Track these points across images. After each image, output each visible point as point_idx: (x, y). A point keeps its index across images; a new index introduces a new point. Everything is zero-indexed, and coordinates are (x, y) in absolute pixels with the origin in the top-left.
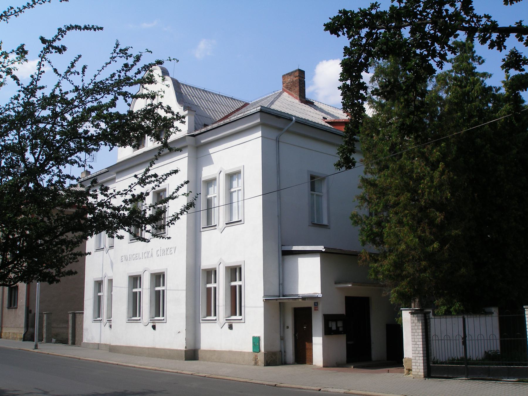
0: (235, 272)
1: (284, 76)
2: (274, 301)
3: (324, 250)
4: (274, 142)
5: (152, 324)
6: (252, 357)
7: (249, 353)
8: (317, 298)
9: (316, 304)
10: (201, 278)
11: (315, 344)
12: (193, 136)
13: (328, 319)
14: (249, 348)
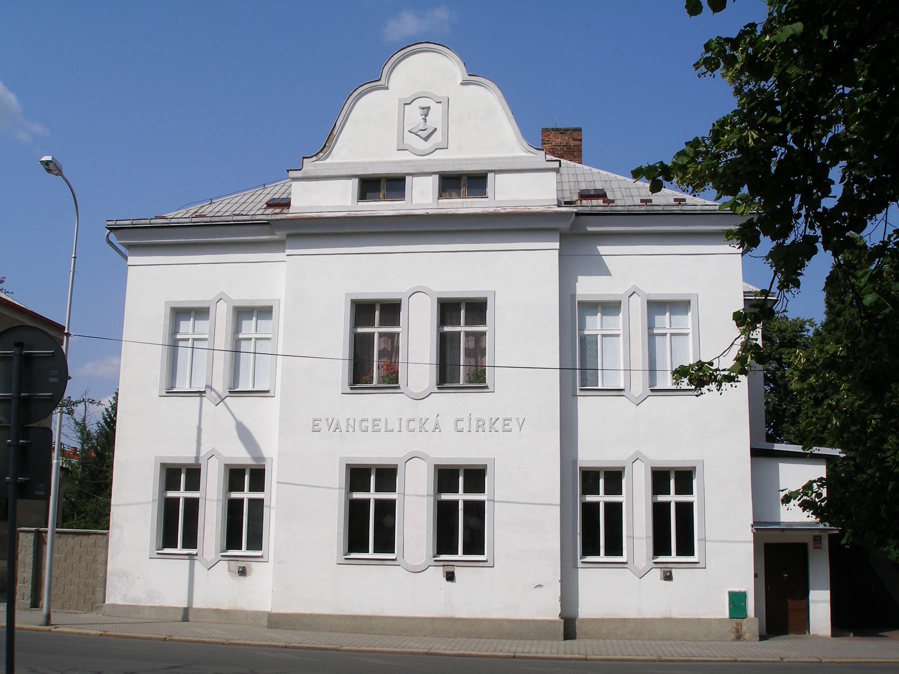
2: (808, 532)
7: (720, 620)
11: (815, 601)
14: (723, 611)
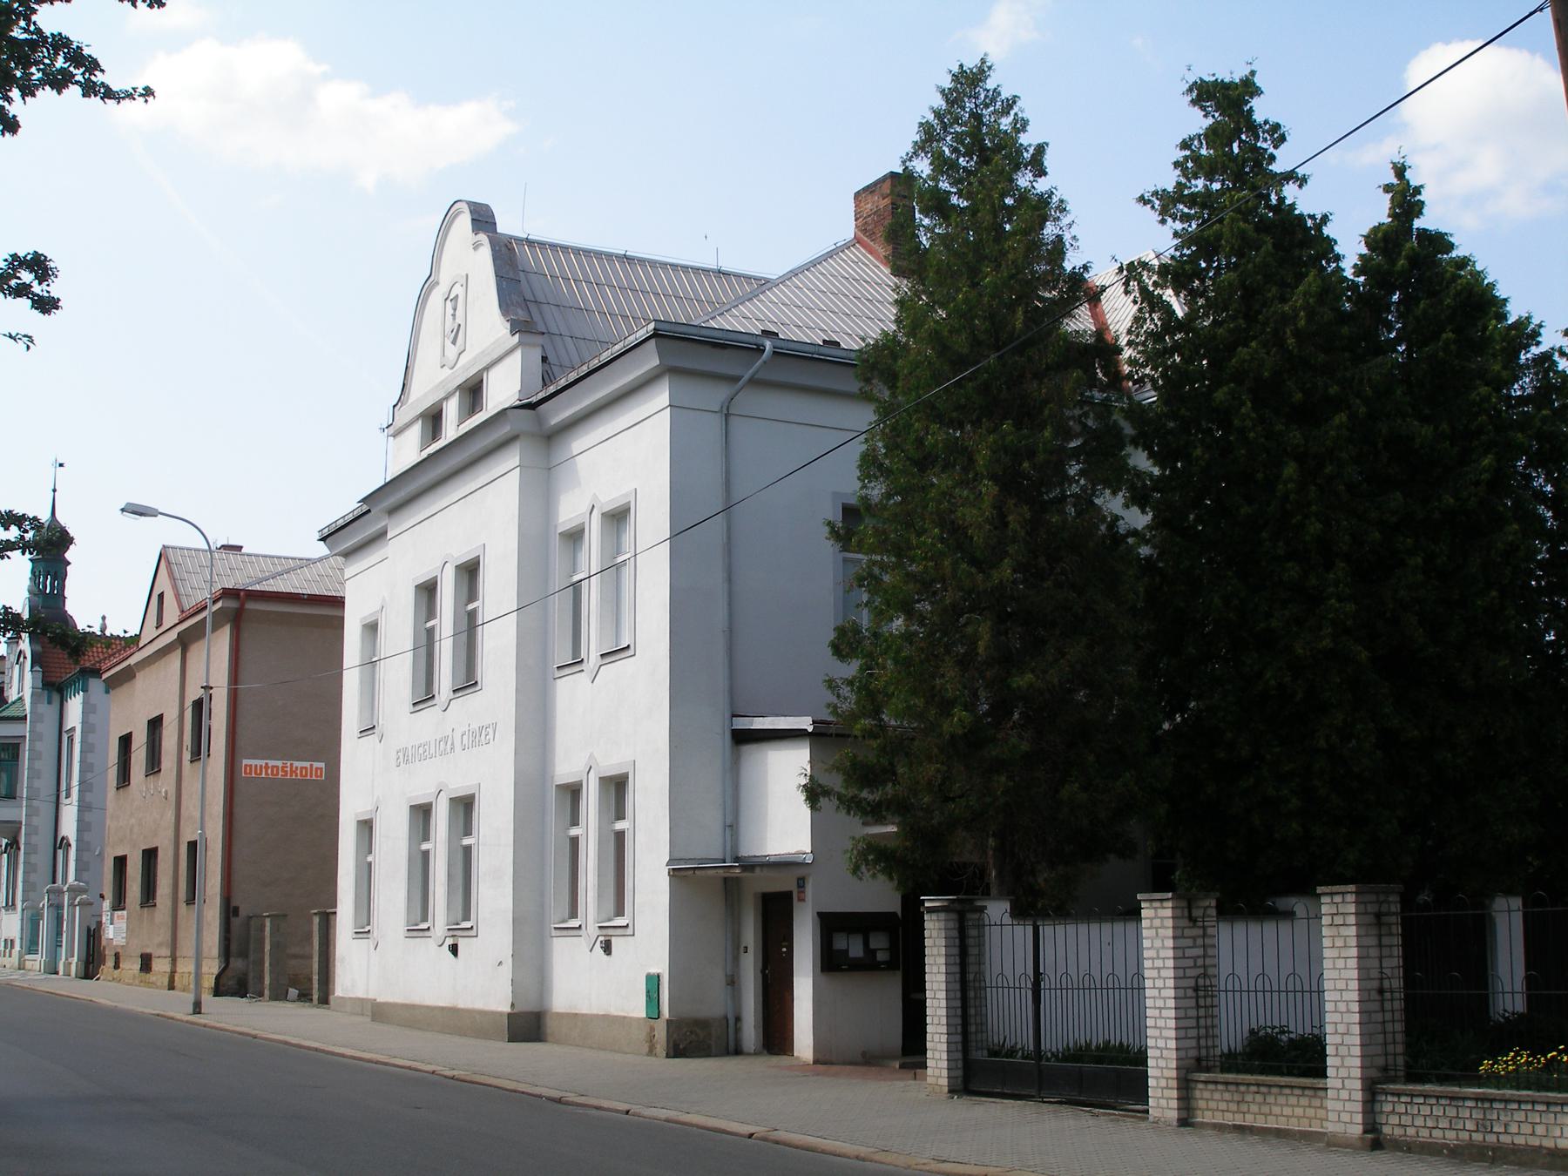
0: (617, 787)
1: (857, 195)
3: (810, 729)
4: (716, 422)
5: (450, 941)
6: (642, 1035)
8: (803, 864)
9: (801, 883)
10: (552, 803)
12: (531, 406)
13: (830, 924)
14: (637, 1008)
